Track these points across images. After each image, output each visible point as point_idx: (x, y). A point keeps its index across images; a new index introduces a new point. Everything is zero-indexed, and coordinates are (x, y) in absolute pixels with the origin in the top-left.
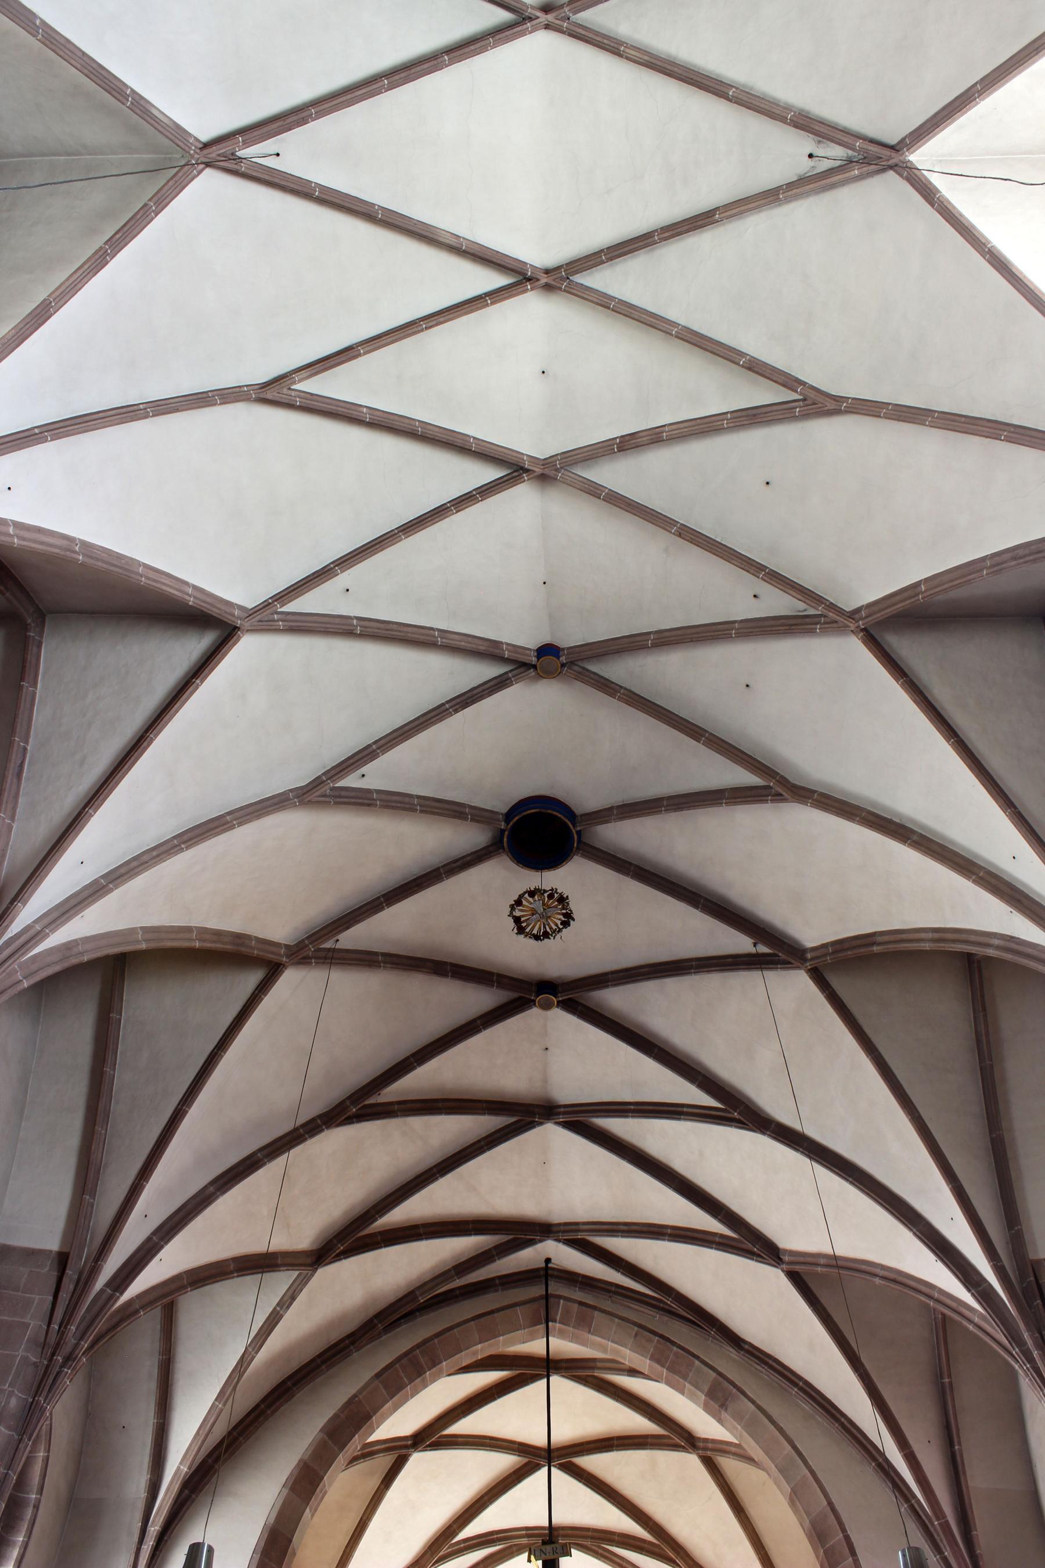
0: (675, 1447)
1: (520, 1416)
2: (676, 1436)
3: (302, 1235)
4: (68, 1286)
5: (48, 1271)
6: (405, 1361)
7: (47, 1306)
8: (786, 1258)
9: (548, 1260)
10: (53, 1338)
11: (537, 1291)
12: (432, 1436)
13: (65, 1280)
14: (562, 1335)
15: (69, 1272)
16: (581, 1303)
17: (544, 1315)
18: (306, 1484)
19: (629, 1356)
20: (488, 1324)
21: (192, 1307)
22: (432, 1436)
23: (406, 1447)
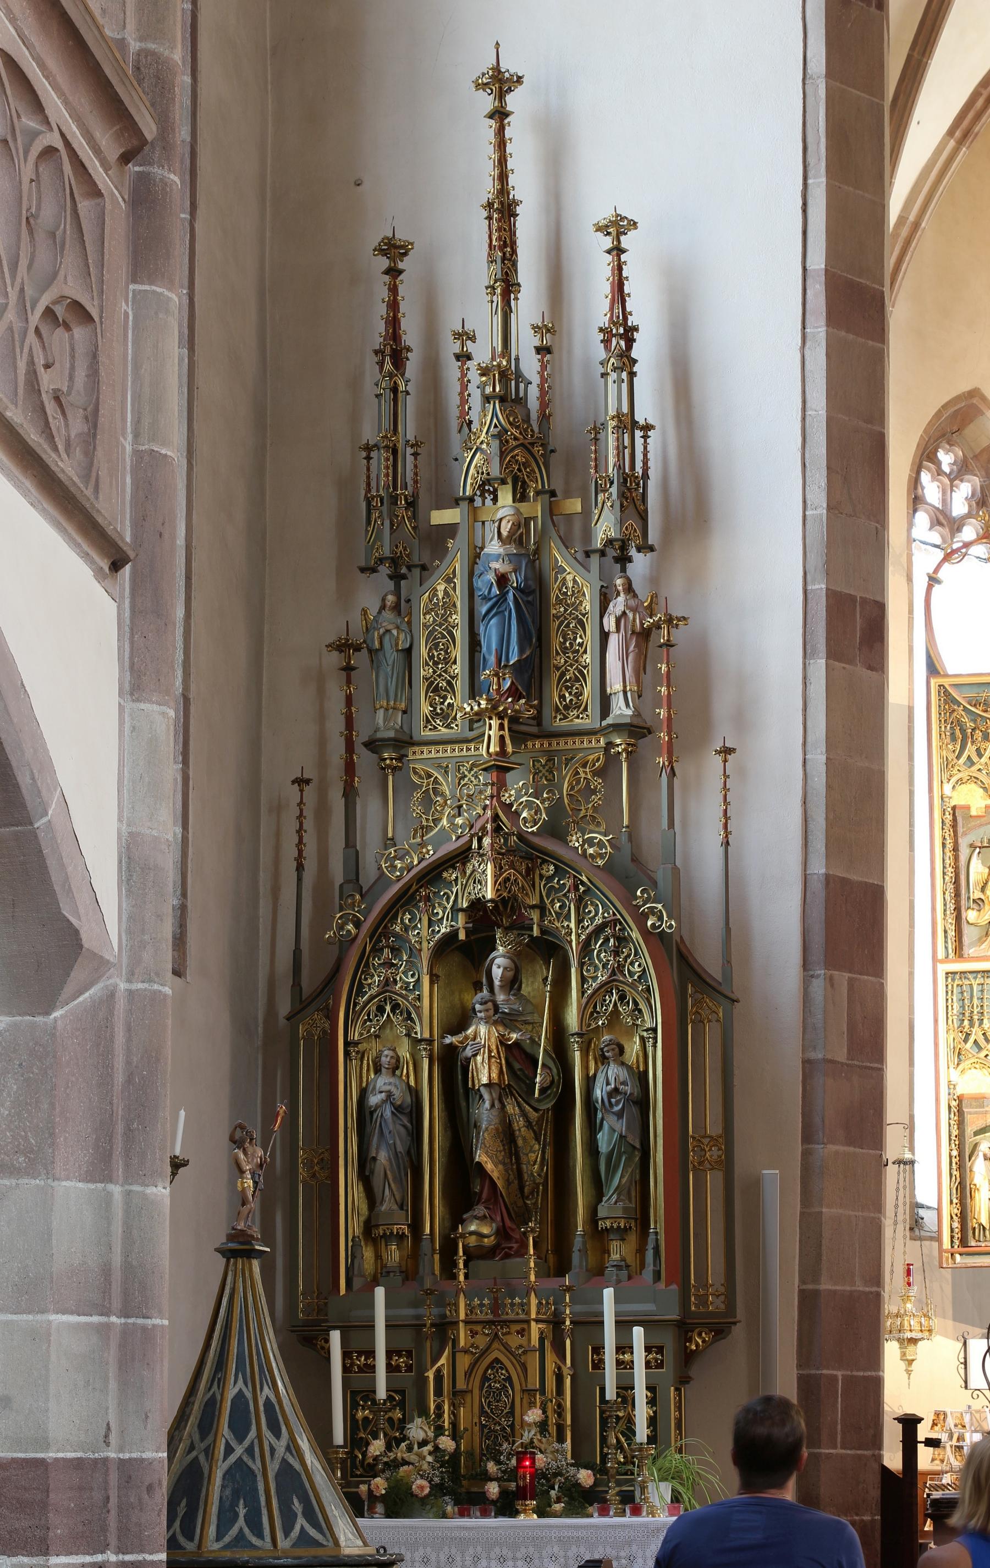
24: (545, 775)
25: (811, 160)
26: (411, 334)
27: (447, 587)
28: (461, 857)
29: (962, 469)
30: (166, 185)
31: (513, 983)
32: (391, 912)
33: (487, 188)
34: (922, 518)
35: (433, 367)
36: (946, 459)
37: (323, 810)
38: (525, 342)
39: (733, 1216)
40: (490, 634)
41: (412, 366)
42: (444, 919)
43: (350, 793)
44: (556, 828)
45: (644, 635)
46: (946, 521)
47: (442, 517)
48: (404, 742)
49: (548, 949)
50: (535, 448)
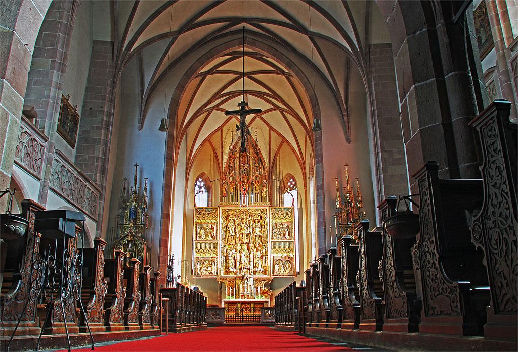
0: (279, 74)
1: (236, 65)
2: (279, 71)
3: (175, 28)
4: (116, 51)
5: (109, 47)
6: (204, 56)
7: (111, 57)
8: (309, 33)
9: (244, 27)
10: (115, 65)
11: (241, 36)
12: (212, 71)
13: (115, 49)
14: (247, 47)
15: (115, 47)
16: (253, 39)
17: (243, 43)
18: (181, 88)
19: (265, 53)
20: (227, 45)
21: (146, 52)
22: (212, 71)
23: (206, 74)
24: (136, 229)
25: (192, 92)
26: (127, 187)
27: (128, 210)
28: (127, 236)
29: (202, 181)
30: (69, 123)
31: (131, 247)
32: (120, 241)
33: (135, 174)
34: (197, 186)
35: (128, 190)
36: (200, 180)
37: (115, 231)
38: (137, 189)
39: (137, 7)
40: (131, 215)
41: (126, 190)
42: (125, 242)
43: (117, 229)
44: (136, 234)
45: (146, 216)
46: (200, 187)
47: (128, 204)
48: (123, 224)
49: (135, 245)
50: (138, 198)
